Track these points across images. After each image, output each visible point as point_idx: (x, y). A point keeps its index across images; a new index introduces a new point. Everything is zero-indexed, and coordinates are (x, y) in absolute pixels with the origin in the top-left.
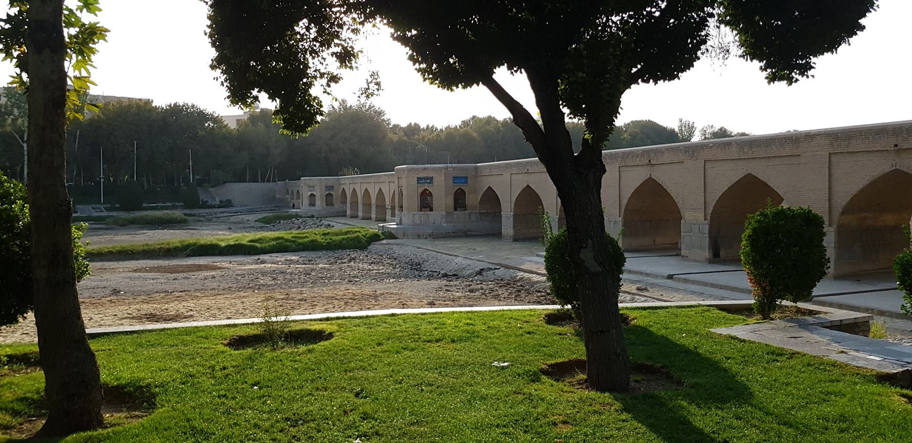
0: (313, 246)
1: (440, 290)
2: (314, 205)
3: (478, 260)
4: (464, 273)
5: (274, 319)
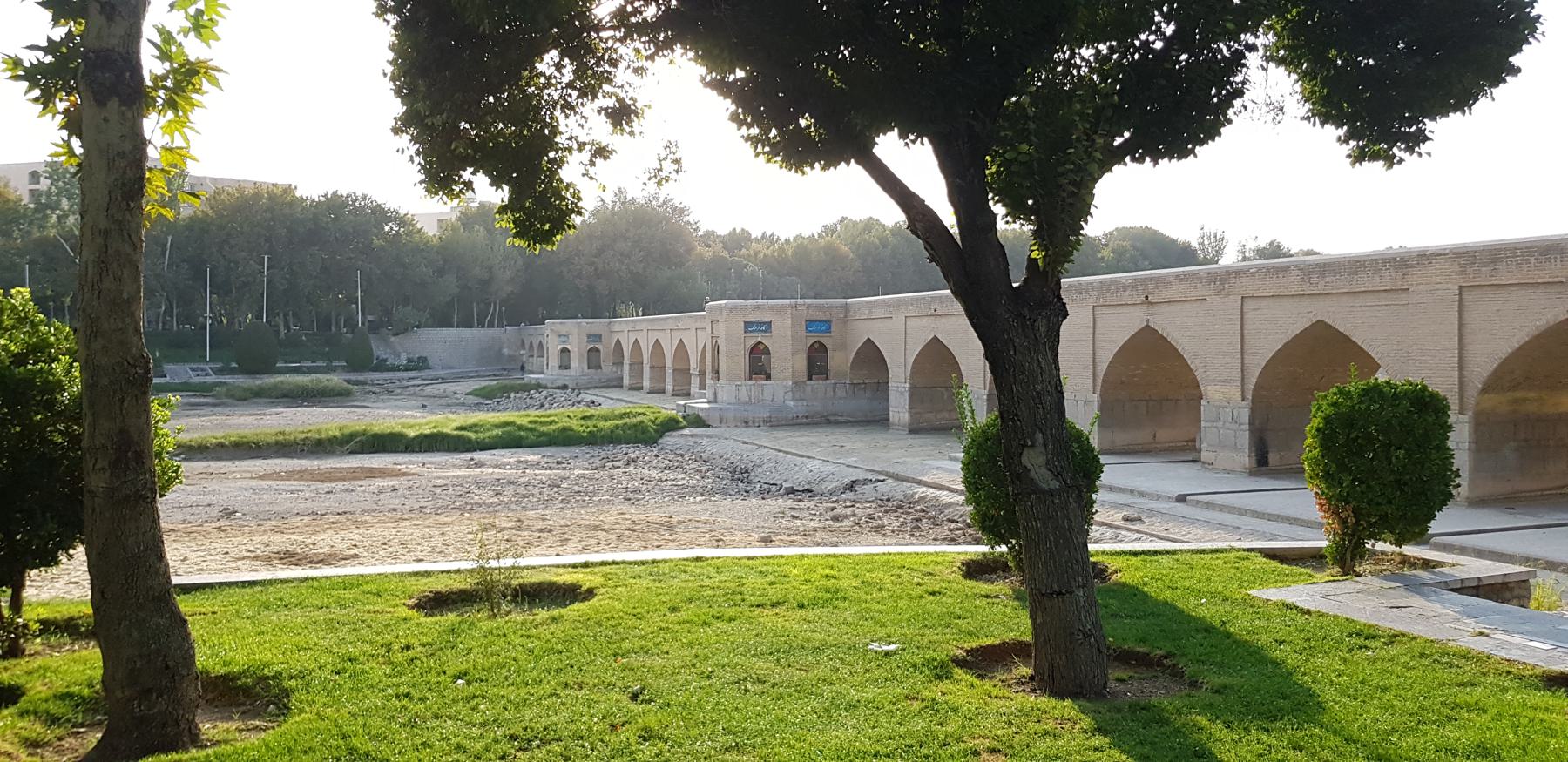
0: (565, 439)
2: (567, 367)
3: (848, 466)
5: (494, 564)
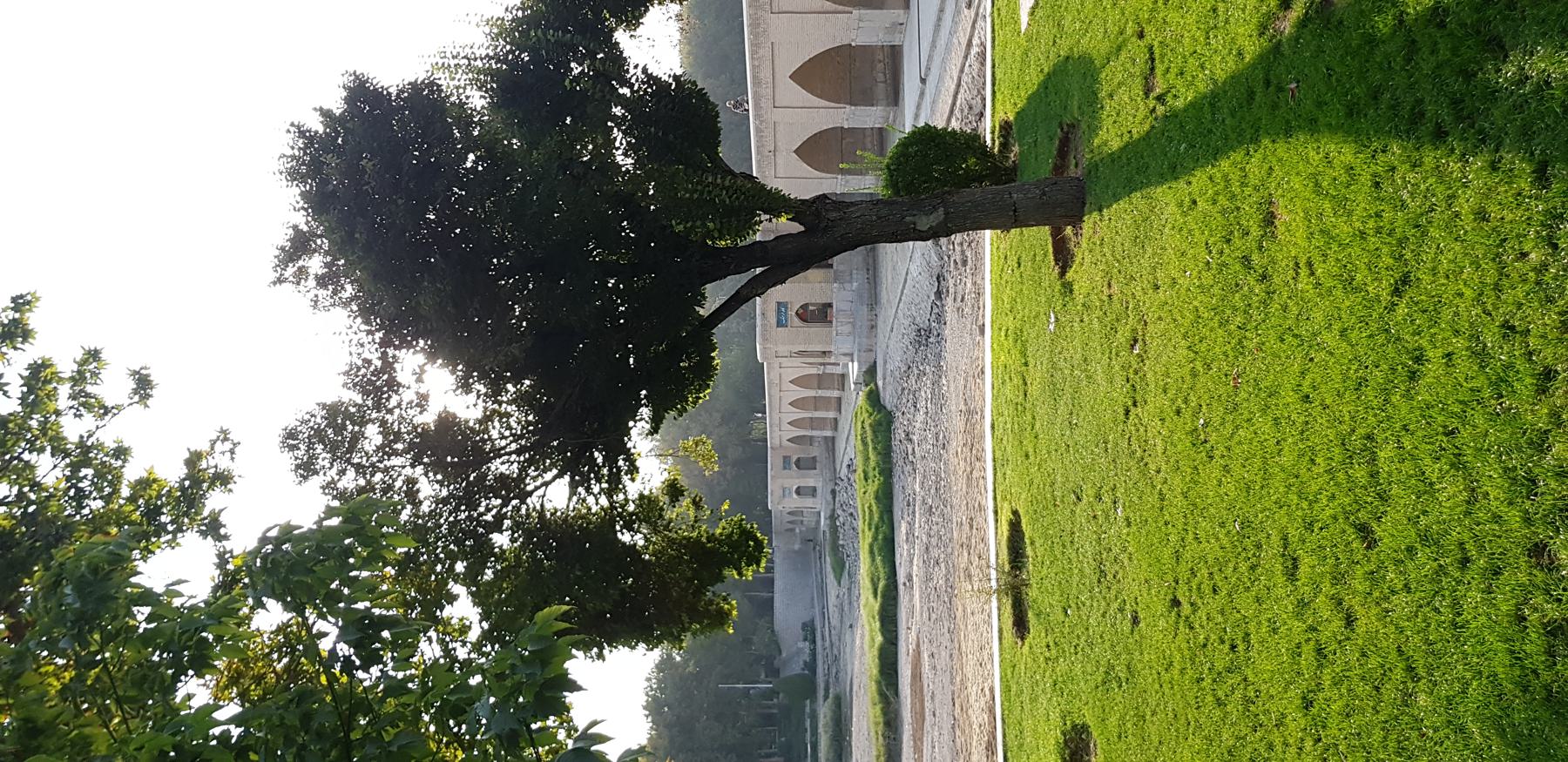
0: (886, 498)
2: (815, 489)
5: (994, 583)
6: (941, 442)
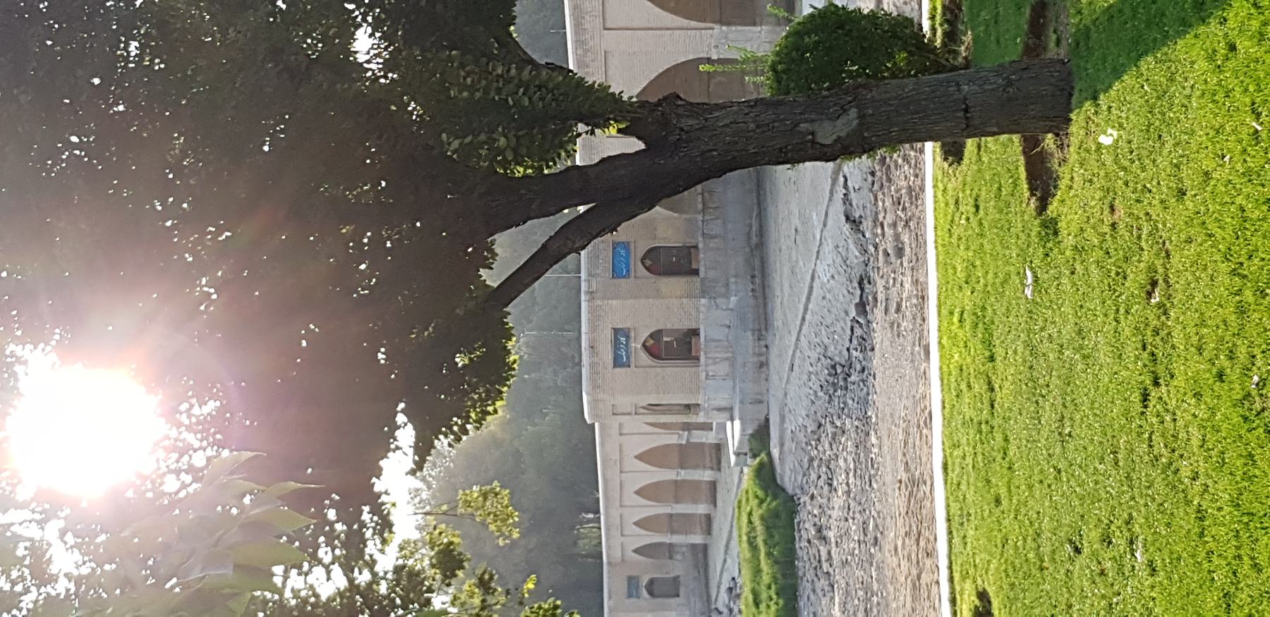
1: (898, 327)
3: (825, 225)
4: (856, 261)
6: (870, 536)
